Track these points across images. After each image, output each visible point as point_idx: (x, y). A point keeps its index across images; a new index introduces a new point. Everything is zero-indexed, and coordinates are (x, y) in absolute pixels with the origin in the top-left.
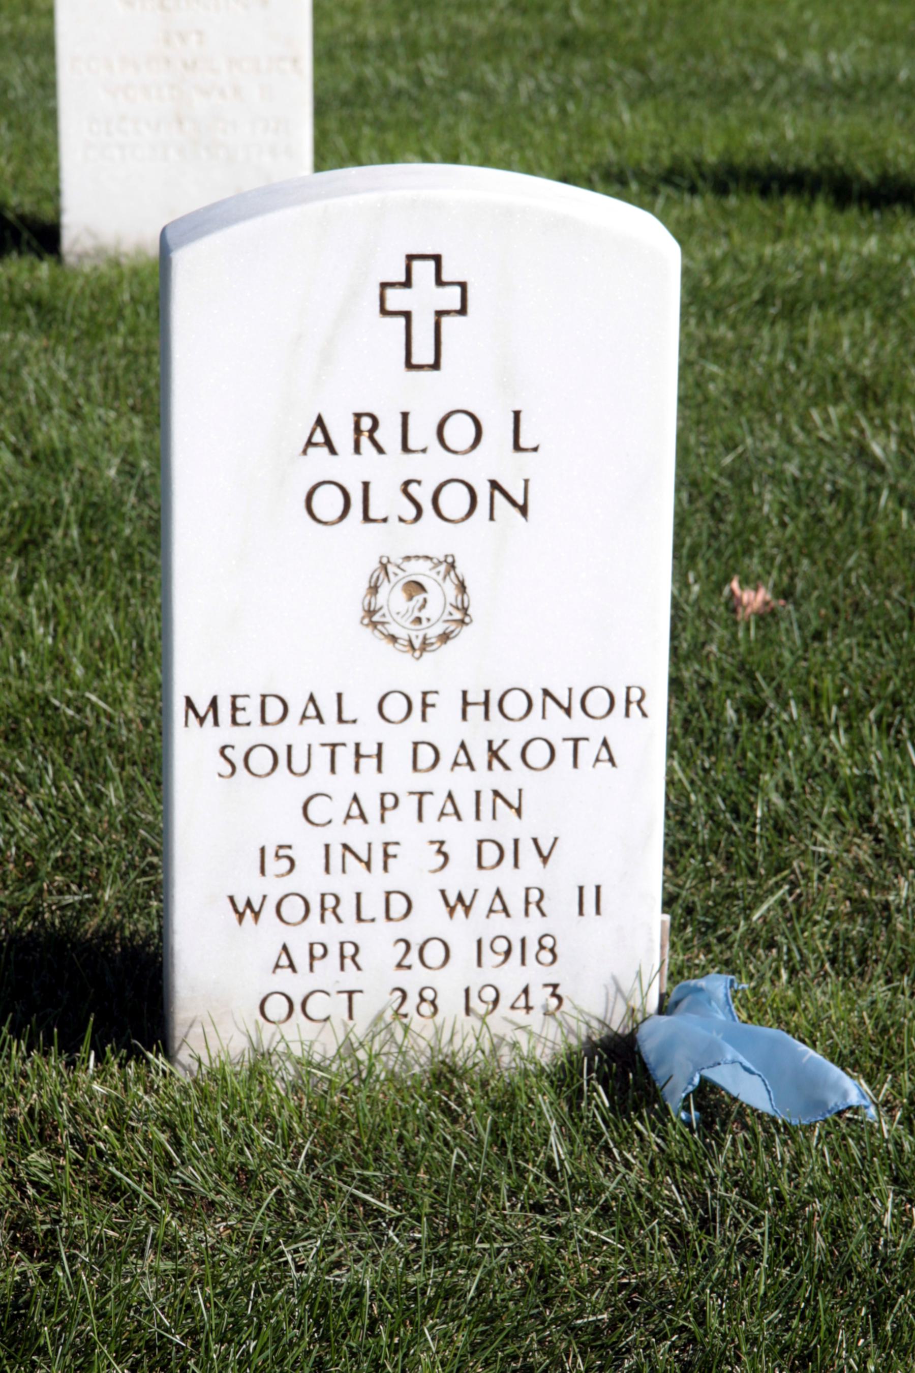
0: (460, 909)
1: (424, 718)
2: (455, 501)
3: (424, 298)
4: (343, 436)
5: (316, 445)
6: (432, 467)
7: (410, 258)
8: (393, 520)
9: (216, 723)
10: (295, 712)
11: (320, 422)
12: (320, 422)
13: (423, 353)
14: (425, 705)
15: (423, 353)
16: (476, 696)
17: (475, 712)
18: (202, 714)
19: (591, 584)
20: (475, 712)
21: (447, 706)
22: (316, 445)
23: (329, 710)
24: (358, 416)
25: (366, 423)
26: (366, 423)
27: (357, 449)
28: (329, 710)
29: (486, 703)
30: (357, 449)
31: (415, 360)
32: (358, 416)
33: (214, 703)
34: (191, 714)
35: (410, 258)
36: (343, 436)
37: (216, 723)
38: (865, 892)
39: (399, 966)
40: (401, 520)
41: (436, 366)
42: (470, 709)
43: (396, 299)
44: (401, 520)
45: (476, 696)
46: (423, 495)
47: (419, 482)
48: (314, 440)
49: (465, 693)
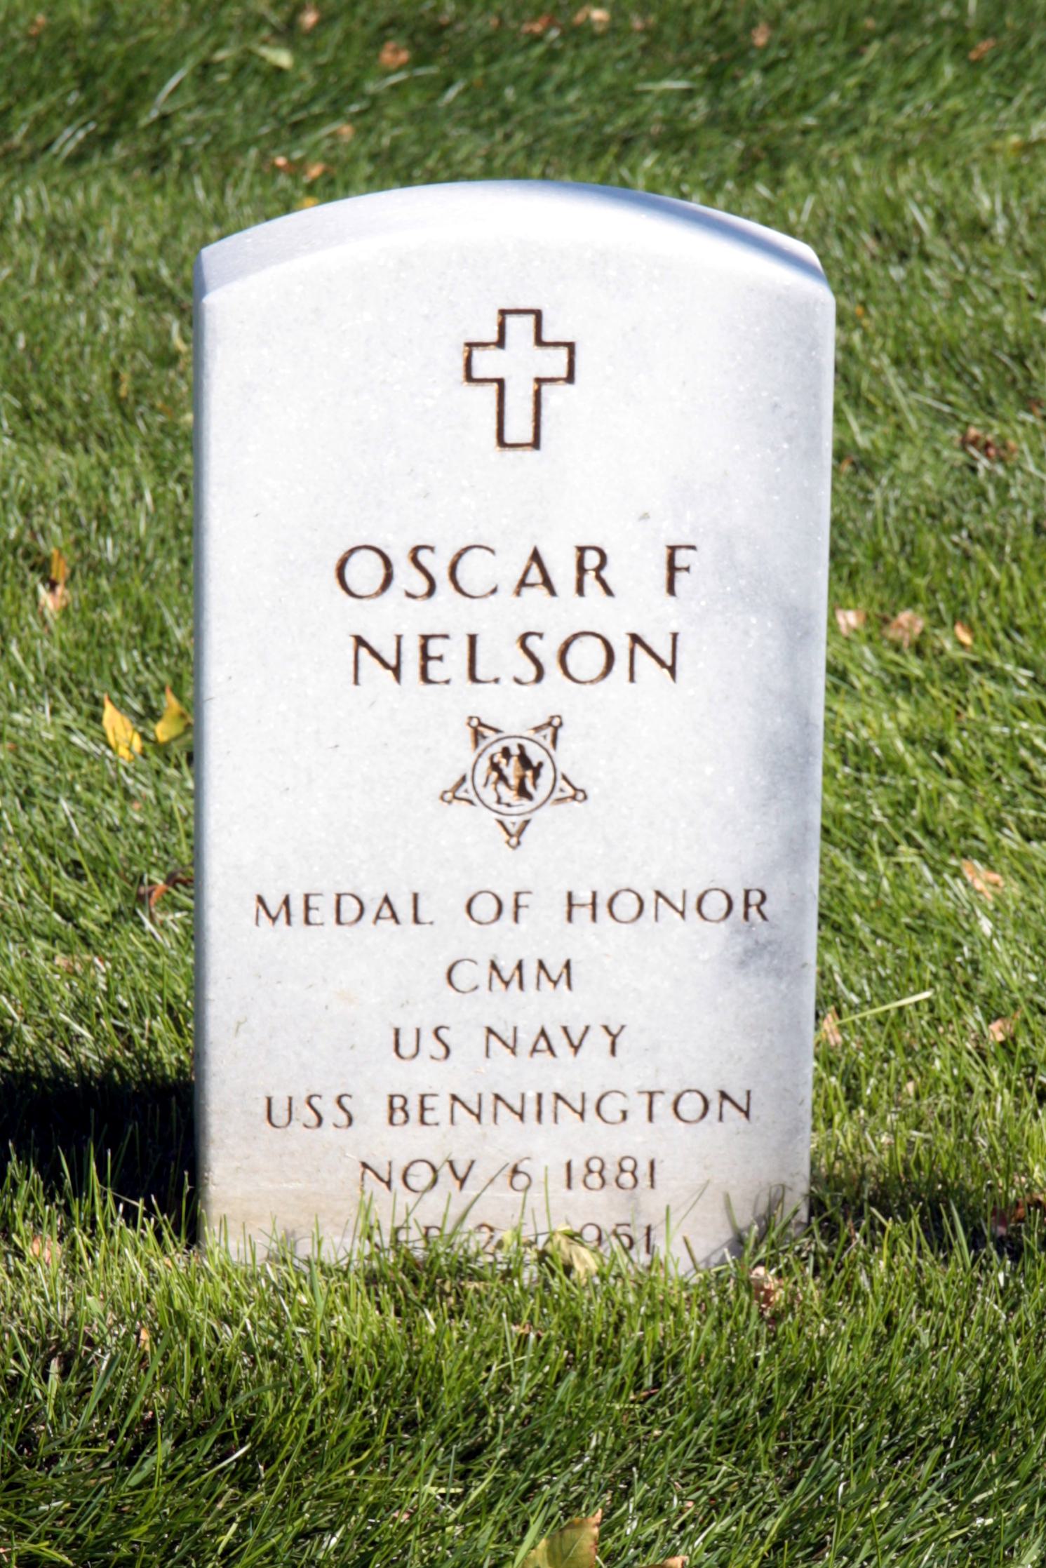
2: (587, 657)
3: (520, 362)
4: (563, 574)
5: (532, 585)
6: (555, 615)
7: (571, 347)
8: (507, 681)
9: (289, 922)
11: (536, 557)
12: (536, 557)
13: (518, 428)
14: (517, 906)
15: (518, 428)
16: (583, 896)
17: (582, 914)
18: (273, 913)
19: (700, 764)
20: (582, 914)
21: (545, 911)
22: (532, 585)
23: (405, 911)
25: (592, 559)
26: (592, 559)
27: (580, 590)
28: (405, 911)
29: (594, 904)
30: (580, 590)
31: (509, 438)
32: (582, 550)
33: (286, 902)
34: (262, 913)
35: (571, 347)
36: (563, 574)
37: (289, 922)
38: (501, 1452)
40: (518, 681)
41: (536, 444)
42: (575, 910)
44: (518, 681)
45: (583, 896)
46: (546, 650)
47: (540, 635)
48: (530, 580)
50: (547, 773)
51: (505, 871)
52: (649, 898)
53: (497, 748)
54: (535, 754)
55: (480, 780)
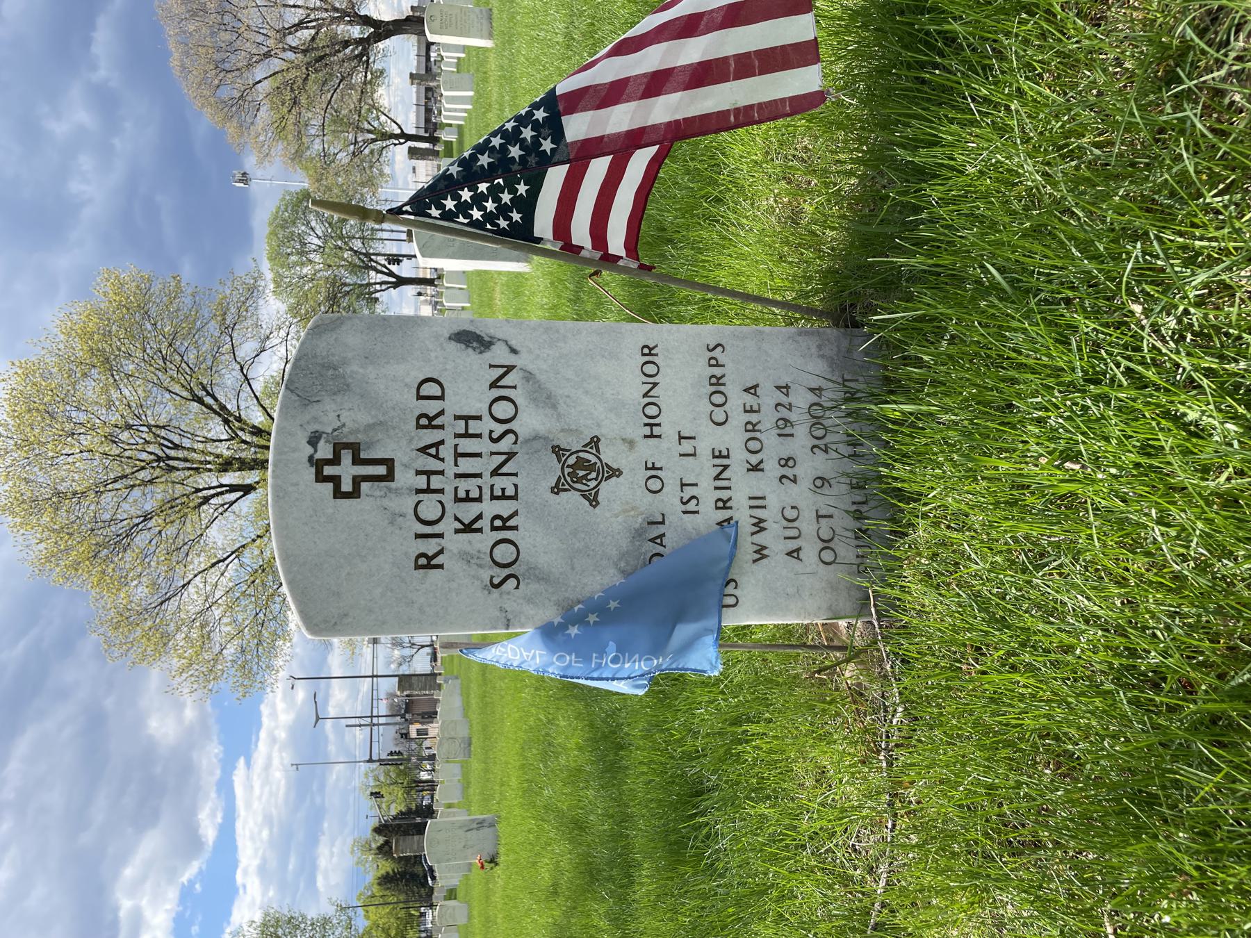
0: (765, 552)
1: (661, 469)
3: (347, 471)
10: (784, 400)
13: (381, 470)
14: (654, 468)
15: (381, 470)
16: (647, 431)
17: (656, 430)
20: (656, 430)
24: (419, 427)
39: (795, 481)
43: (347, 486)
45: (647, 431)
49: (646, 437)
50: (581, 455)
51: (633, 476)
52: (647, 400)
53: (568, 479)
54: (572, 460)
55: (585, 488)
